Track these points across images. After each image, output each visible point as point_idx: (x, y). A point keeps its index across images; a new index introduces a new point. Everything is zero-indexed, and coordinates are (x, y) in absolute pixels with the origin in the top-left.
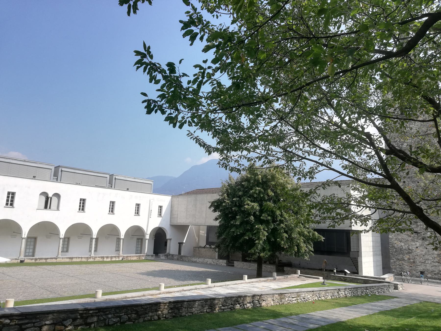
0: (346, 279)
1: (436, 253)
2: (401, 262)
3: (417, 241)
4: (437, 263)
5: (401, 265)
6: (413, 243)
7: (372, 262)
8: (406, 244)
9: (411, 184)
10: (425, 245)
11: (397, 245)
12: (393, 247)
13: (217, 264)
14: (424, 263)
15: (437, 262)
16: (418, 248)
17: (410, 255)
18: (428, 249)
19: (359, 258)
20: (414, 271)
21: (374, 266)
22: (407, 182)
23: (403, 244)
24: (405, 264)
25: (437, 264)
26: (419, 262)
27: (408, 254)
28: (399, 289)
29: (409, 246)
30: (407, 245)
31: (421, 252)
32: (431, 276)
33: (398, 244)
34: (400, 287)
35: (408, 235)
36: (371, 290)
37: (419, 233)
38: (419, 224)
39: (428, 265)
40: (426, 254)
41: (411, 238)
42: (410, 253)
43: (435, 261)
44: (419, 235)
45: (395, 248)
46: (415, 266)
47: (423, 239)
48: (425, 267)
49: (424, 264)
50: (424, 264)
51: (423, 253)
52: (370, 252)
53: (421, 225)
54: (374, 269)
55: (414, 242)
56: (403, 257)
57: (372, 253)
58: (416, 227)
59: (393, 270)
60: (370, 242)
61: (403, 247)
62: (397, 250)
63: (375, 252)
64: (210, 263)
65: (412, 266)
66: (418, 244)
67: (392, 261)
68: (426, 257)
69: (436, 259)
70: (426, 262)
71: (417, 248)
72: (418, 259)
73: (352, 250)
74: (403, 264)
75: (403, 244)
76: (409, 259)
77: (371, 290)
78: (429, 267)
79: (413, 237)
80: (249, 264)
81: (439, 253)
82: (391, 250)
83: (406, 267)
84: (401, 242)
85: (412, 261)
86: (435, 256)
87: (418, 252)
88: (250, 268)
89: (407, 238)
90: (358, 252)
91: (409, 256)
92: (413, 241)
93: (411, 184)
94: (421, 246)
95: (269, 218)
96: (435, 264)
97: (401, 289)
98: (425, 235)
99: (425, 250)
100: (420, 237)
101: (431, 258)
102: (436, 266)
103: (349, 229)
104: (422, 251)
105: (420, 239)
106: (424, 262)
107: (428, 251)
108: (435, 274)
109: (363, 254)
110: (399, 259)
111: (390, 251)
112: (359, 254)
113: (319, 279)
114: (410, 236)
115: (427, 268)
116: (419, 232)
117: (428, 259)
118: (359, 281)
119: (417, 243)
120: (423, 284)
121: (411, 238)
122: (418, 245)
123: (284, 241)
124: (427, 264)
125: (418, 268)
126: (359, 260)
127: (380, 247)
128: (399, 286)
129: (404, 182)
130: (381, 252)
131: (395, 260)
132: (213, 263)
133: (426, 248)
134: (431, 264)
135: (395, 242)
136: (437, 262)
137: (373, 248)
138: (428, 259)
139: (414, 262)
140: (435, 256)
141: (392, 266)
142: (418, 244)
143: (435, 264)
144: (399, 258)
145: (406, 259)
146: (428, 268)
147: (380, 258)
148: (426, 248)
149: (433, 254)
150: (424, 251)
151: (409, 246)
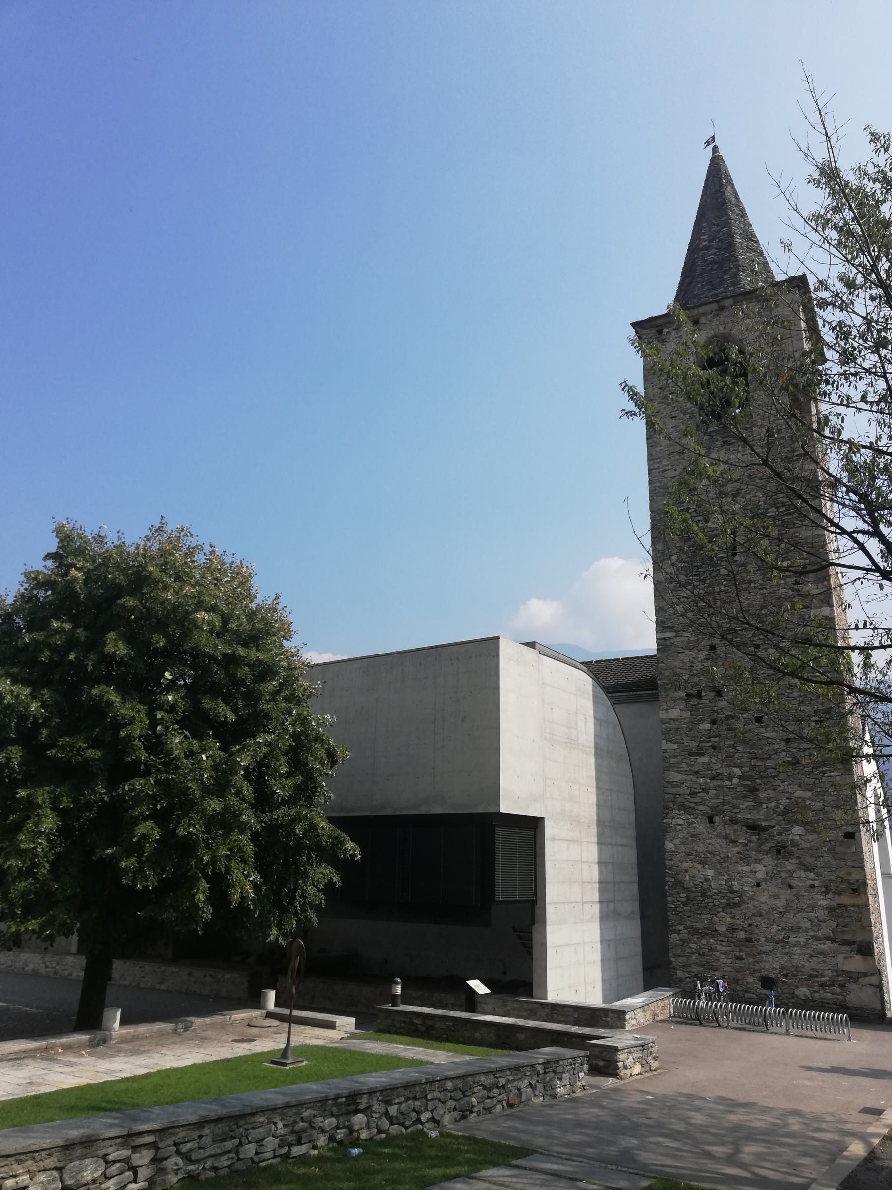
0: (431, 1028)
1: (824, 903)
2: (704, 941)
3: (758, 861)
4: (828, 943)
5: (704, 955)
6: (745, 868)
7: (598, 946)
8: (720, 874)
9: (735, 654)
10: (784, 875)
11: (693, 877)
12: (679, 883)
13: (55, 973)
14: (784, 942)
15: (828, 938)
16: (763, 885)
17: (736, 912)
18: (794, 891)
19: (535, 928)
20: (751, 974)
21: (603, 961)
22: (720, 649)
23: (710, 873)
24: (719, 947)
25: (827, 946)
26: (767, 940)
27: (729, 910)
28: (623, 1072)
29: (731, 878)
30: (726, 878)
31: (772, 902)
32: (808, 993)
33: (695, 872)
34: (629, 1062)
35: (726, 837)
36: (393, 1110)
37: (765, 829)
38: (762, 795)
39: (797, 950)
40: (788, 907)
41: (737, 849)
42: (737, 905)
43: (820, 934)
44: (764, 835)
45: (687, 890)
46: (754, 956)
47: (778, 852)
48: (787, 958)
49: (783, 947)
50: (783, 947)
51: (780, 904)
52: (587, 906)
53: (769, 800)
54: (603, 971)
55: (749, 865)
56: (711, 922)
57: (596, 908)
58: (754, 808)
59: (680, 974)
60: (585, 866)
61: (713, 883)
62: (693, 895)
63: (611, 906)
64: (33, 970)
65: (743, 954)
66: (761, 871)
67: (674, 938)
68: (792, 919)
69: (823, 925)
70: (792, 939)
71: (758, 885)
72: (763, 927)
73: (499, 897)
74: (711, 949)
75: (710, 873)
76: (732, 929)
77: (393, 1110)
78: (800, 958)
79: (745, 845)
80: (163, 969)
81: (834, 904)
82: (672, 895)
83: (723, 959)
84: (703, 863)
85: (742, 935)
86: (822, 914)
87: (763, 900)
88: (163, 987)
89: (725, 850)
90: (533, 903)
91: (733, 918)
92: (744, 858)
93: (735, 654)
94: (772, 876)
95: (93, 753)
96: (821, 946)
97: (637, 1069)
98: (784, 837)
99: (786, 895)
100: (769, 845)
101: (808, 924)
102: (825, 956)
103: (491, 810)
104: (776, 897)
105: (767, 853)
106: (782, 941)
107: (797, 897)
108: (822, 985)
109: (552, 913)
110: (696, 932)
111: (669, 899)
112: (537, 911)
113: (331, 1026)
114: (734, 842)
115: (795, 962)
116: (764, 824)
117: (796, 929)
118: (477, 1035)
119: (759, 867)
120: (771, 1029)
121: (737, 849)
122: (760, 875)
123: (140, 856)
124: (795, 945)
125: (762, 965)
126: (536, 937)
127: (635, 888)
128: (622, 1056)
129: (713, 647)
130: (637, 905)
131: (685, 934)
132: (43, 971)
133: (791, 887)
134: (806, 945)
135: (686, 865)
136: (828, 938)
137: (601, 890)
138: (796, 929)
139: (749, 940)
140: (822, 914)
141: (675, 956)
142: (761, 871)
143: (821, 946)
144: (698, 925)
145: (722, 929)
146: (798, 961)
147: (632, 930)
148: (791, 887)
149: (813, 908)
150: (784, 897)
151: (731, 878)
